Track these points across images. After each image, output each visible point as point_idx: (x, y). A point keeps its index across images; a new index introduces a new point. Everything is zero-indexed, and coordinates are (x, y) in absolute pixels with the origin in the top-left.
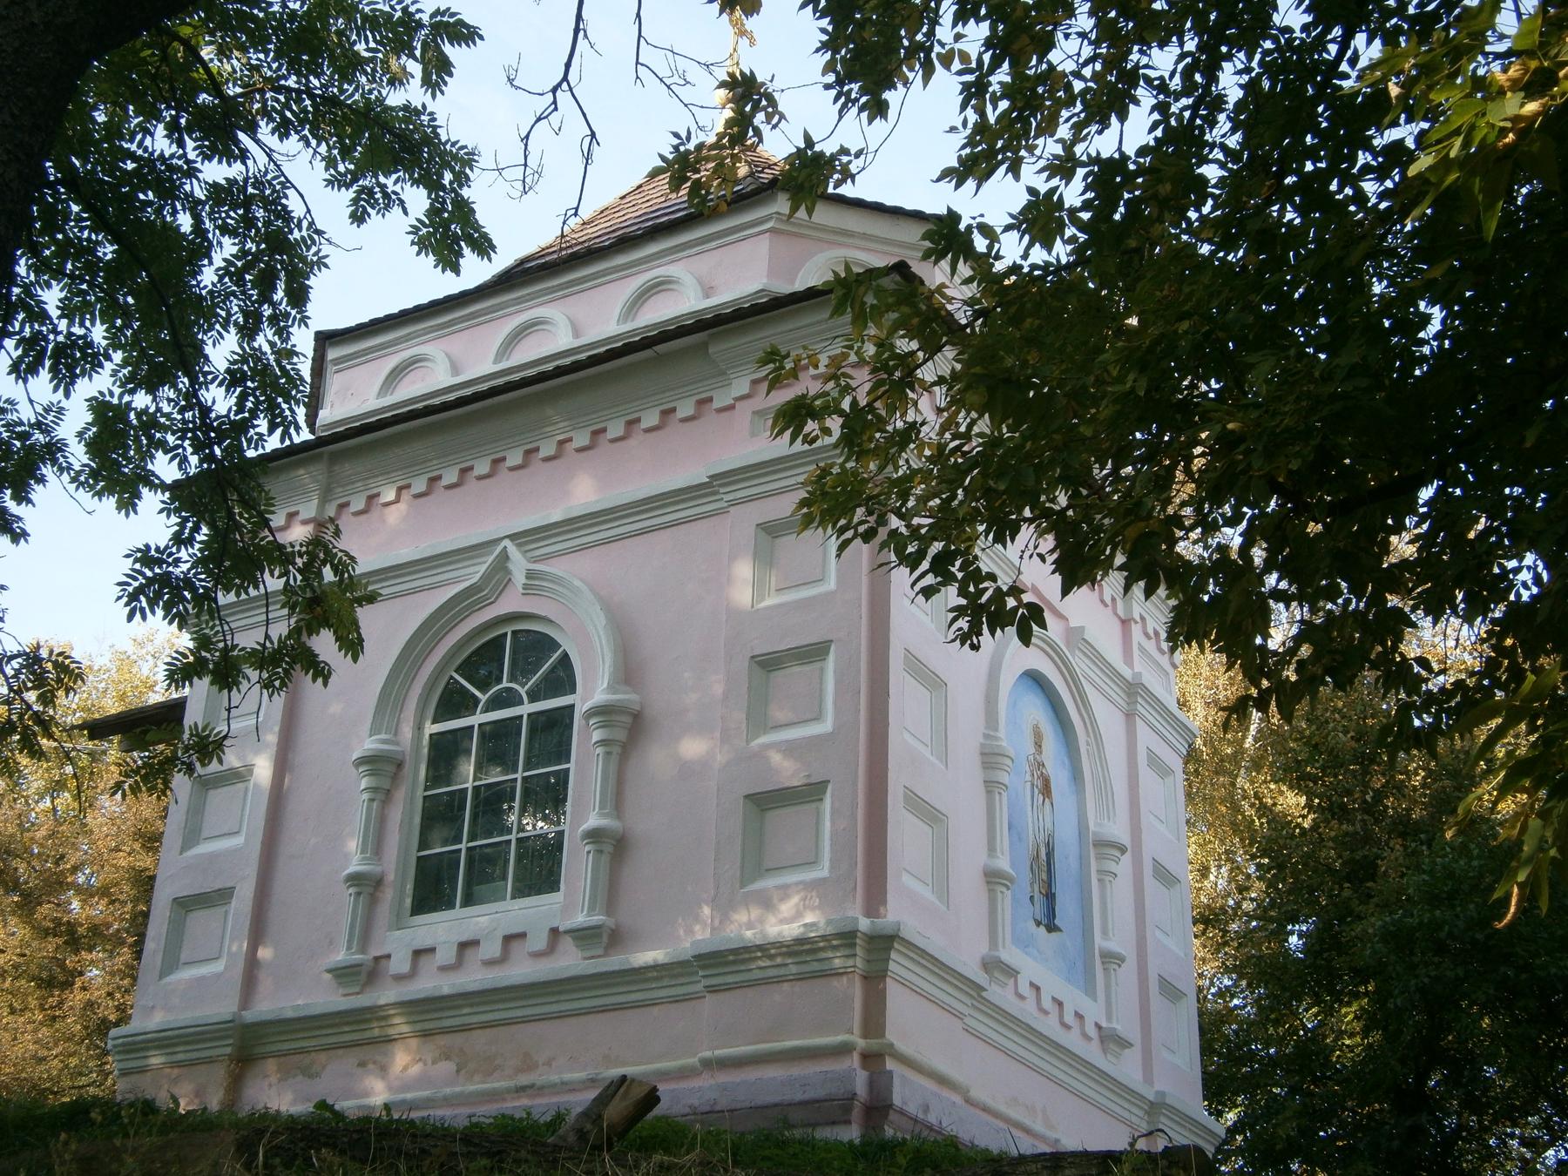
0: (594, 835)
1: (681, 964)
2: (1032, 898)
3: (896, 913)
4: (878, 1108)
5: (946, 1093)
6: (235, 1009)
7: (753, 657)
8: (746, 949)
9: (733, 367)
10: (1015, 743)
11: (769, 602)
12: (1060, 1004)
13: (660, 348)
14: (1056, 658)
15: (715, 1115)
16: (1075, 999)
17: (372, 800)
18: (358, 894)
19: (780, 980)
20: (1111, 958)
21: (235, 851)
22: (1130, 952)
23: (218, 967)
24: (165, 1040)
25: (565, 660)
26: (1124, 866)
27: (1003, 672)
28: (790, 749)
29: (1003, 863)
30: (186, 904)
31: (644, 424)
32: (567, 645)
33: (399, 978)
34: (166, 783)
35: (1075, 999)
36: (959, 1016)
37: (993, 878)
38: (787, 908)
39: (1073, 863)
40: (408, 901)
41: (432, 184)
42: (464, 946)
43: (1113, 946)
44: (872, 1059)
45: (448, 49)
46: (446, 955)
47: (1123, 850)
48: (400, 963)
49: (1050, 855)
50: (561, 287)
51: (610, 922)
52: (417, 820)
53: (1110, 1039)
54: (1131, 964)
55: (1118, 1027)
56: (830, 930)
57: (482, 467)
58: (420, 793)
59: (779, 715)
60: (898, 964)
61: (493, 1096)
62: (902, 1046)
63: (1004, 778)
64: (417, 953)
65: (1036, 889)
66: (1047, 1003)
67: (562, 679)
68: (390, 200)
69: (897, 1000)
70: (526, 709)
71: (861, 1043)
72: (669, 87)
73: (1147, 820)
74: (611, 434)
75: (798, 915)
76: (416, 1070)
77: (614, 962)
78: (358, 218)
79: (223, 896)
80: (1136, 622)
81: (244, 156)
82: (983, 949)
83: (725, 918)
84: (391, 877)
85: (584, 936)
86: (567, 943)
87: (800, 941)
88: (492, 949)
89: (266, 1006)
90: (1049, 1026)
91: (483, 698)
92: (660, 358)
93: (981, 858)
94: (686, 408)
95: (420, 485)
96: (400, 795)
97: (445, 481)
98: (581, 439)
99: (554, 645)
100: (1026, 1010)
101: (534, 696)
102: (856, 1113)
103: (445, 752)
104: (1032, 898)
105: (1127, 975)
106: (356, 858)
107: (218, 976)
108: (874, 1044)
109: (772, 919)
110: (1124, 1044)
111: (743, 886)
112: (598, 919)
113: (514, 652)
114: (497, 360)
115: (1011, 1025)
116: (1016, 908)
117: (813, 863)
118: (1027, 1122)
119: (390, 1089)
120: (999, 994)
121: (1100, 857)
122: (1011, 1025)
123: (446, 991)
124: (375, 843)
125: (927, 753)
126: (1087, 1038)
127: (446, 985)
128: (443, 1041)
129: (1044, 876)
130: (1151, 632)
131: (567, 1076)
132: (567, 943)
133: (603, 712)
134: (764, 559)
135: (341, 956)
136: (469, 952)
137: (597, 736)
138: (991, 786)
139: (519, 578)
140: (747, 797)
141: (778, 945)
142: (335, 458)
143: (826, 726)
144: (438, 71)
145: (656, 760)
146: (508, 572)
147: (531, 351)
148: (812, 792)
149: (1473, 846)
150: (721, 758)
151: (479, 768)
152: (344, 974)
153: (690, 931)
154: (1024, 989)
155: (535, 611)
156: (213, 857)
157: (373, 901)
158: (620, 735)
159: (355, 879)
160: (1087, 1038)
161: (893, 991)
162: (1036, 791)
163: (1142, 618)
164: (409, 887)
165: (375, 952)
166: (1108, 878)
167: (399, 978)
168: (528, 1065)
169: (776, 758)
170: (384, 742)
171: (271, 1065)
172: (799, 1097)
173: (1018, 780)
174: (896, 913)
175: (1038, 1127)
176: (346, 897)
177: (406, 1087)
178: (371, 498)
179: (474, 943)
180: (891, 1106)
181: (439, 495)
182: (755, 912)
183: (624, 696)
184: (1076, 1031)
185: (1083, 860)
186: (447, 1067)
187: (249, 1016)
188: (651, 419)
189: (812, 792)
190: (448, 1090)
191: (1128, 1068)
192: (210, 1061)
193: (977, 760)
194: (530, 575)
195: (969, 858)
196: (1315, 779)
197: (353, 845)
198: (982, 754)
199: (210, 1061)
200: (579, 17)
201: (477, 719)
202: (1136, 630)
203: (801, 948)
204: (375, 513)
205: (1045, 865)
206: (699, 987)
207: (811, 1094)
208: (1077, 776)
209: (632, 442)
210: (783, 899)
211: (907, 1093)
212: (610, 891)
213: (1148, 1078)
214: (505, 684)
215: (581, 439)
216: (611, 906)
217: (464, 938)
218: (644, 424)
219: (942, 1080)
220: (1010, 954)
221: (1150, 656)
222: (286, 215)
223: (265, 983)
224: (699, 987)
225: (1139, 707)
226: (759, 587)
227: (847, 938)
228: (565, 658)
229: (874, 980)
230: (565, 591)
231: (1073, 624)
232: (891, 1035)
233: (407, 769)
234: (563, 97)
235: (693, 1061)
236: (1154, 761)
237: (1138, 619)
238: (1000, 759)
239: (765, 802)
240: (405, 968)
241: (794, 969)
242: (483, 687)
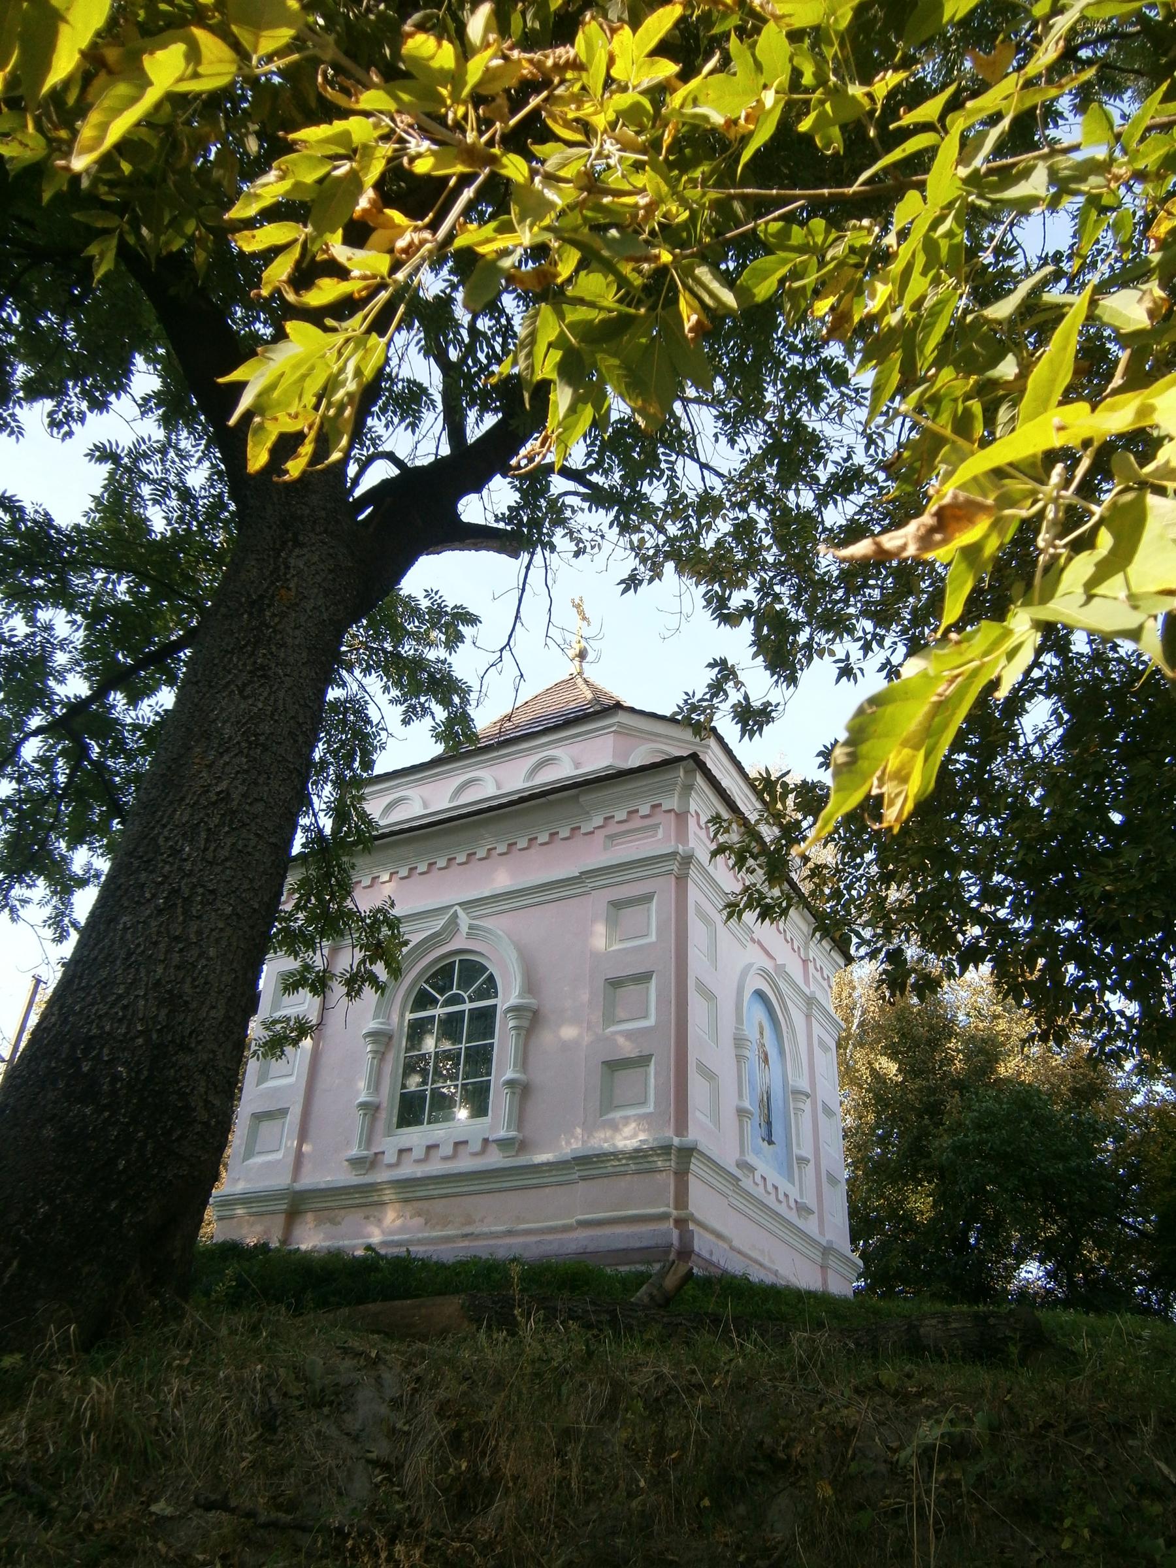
0: (511, 1083)
1: (566, 1162)
3: (694, 1134)
4: (686, 1252)
5: (720, 1243)
6: (288, 1181)
8: (605, 1154)
10: (751, 1033)
11: (615, 947)
12: (776, 1188)
16: (784, 1186)
19: (625, 1174)
20: (802, 1160)
21: (290, 1086)
22: (810, 1156)
23: (278, 1156)
24: (246, 1200)
25: (491, 978)
26: (807, 1106)
28: (629, 1035)
29: (746, 1104)
30: (259, 1118)
31: (540, 841)
32: (492, 969)
33: (390, 1166)
34: (283, 1052)
35: (784, 1186)
36: (725, 1196)
38: (628, 1130)
39: (781, 1104)
40: (395, 1120)
41: (446, 703)
42: (430, 1148)
44: (680, 1223)
45: (461, 627)
46: (418, 1153)
47: (808, 1096)
48: (390, 1157)
49: (768, 1099)
51: (520, 1136)
52: (401, 1071)
53: (803, 1209)
54: (812, 1162)
56: (655, 1144)
57: (442, 863)
58: (402, 1055)
59: (621, 1014)
60: (695, 1165)
61: (447, 1239)
62: (697, 1215)
63: (747, 1053)
64: (401, 1151)
66: (770, 1188)
67: (490, 988)
68: (426, 710)
69: (696, 1188)
70: (467, 1006)
71: (675, 1213)
73: (818, 1078)
74: (519, 846)
75: (635, 1135)
76: (399, 1222)
77: (522, 1160)
78: (406, 722)
79: (283, 1112)
81: (344, 685)
82: (737, 1156)
83: (590, 1135)
84: (385, 1105)
85: (504, 1144)
86: (493, 1148)
87: (637, 1150)
88: (447, 1150)
89: (311, 1179)
90: (771, 1201)
91: (441, 999)
92: (550, 803)
93: (735, 1102)
94: (565, 833)
95: (404, 872)
96: (390, 1056)
97: (419, 870)
98: (502, 848)
99: (485, 969)
100: (759, 1191)
101: (471, 1000)
103: (417, 1030)
105: (810, 1169)
106: (364, 1093)
107: (278, 1161)
108: (682, 1213)
109: (618, 1137)
112: (513, 1134)
113: (460, 971)
114: (451, 800)
116: (753, 1129)
117: (644, 1103)
118: (760, 1258)
119: (383, 1232)
120: (747, 1183)
121: (795, 1100)
123: (419, 1175)
124: (375, 1084)
126: (790, 1208)
127: (419, 1171)
128: (417, 1205)
131: (494, 1229)
132: (493, 1148)
133: (515, 1009)
134: (612, 923)
135: (354, 1152)
136: (433, 1152)
137: (511, 1024)
138: (740, 1058)
139: (464, 929)
141: (622, 1152)
143: (651, 1022)
144: (454, 640)
145: (546, 1038)
146: (457, 925)
147: (471, 796)
148: (642, 1061)
150: (587, 1039)
151: (438, 1040)
152: (357, 1163)
153: (568, 1143)
154: (758, 1179)
155: (735, 986)
157: (374, 1119)
158: (526, 1024)
159: (364, 1106)
160: (790, 1208)
161: (691, 1179)
164: (396, 1111)
167: (390, 1166)
168: (469, 1221)
169: (621, 1040)
171: (310, 1217)
172: (638, 1245)
173: (752, 1054)
174: (694, 1134)
175: (766, 1262)
176: (358, 1116)
177: (392, 1233)
178: (374, 879)
179: (436, 1146)
181: (416, 878)
182: (609, 1133)
184: (784, 1205)
186: (419, 1221)
187: (298, 1186)
188: (544, 837)
189: (642, 1061)
190: (420, 1235)
191: (810, 1226)
192: (273, 1213)
193: (732, 1042)
194: (471, 927)
195: (729, 1102)
197: (362, 1084)
199: (273, 1213)
200: (518, 611)
201: (439, 1011)
202: (811, 965)
203: (637, 1155)
204: (376, 887)
205: (766, 1104)
206: (576, 1176)
207: (644, 1244)
208: (782, 1052)
209: (532, 851)
210: (626, 1125)
211: (702, 1244)
212: (519, 1118)
213: (822, 1233)
215: (502, 848)
216: (519, 1128)
217: (430, 1143)
218: (540, 841)
219: (719, 1236)
220: (751, 1159)
222: (368, 721)
223: (307, 1167)
226: (609, 938)
227: (666, 1149)
228: (491, 977)
229: (682, 1175)
232: (692, 1208)
233: (395, 1040)
234: (506, 653)
235: (573, 1221)
239: (614, 1066)
240: (394, 1160)
241: (633, 1167)
242: (442, 993)
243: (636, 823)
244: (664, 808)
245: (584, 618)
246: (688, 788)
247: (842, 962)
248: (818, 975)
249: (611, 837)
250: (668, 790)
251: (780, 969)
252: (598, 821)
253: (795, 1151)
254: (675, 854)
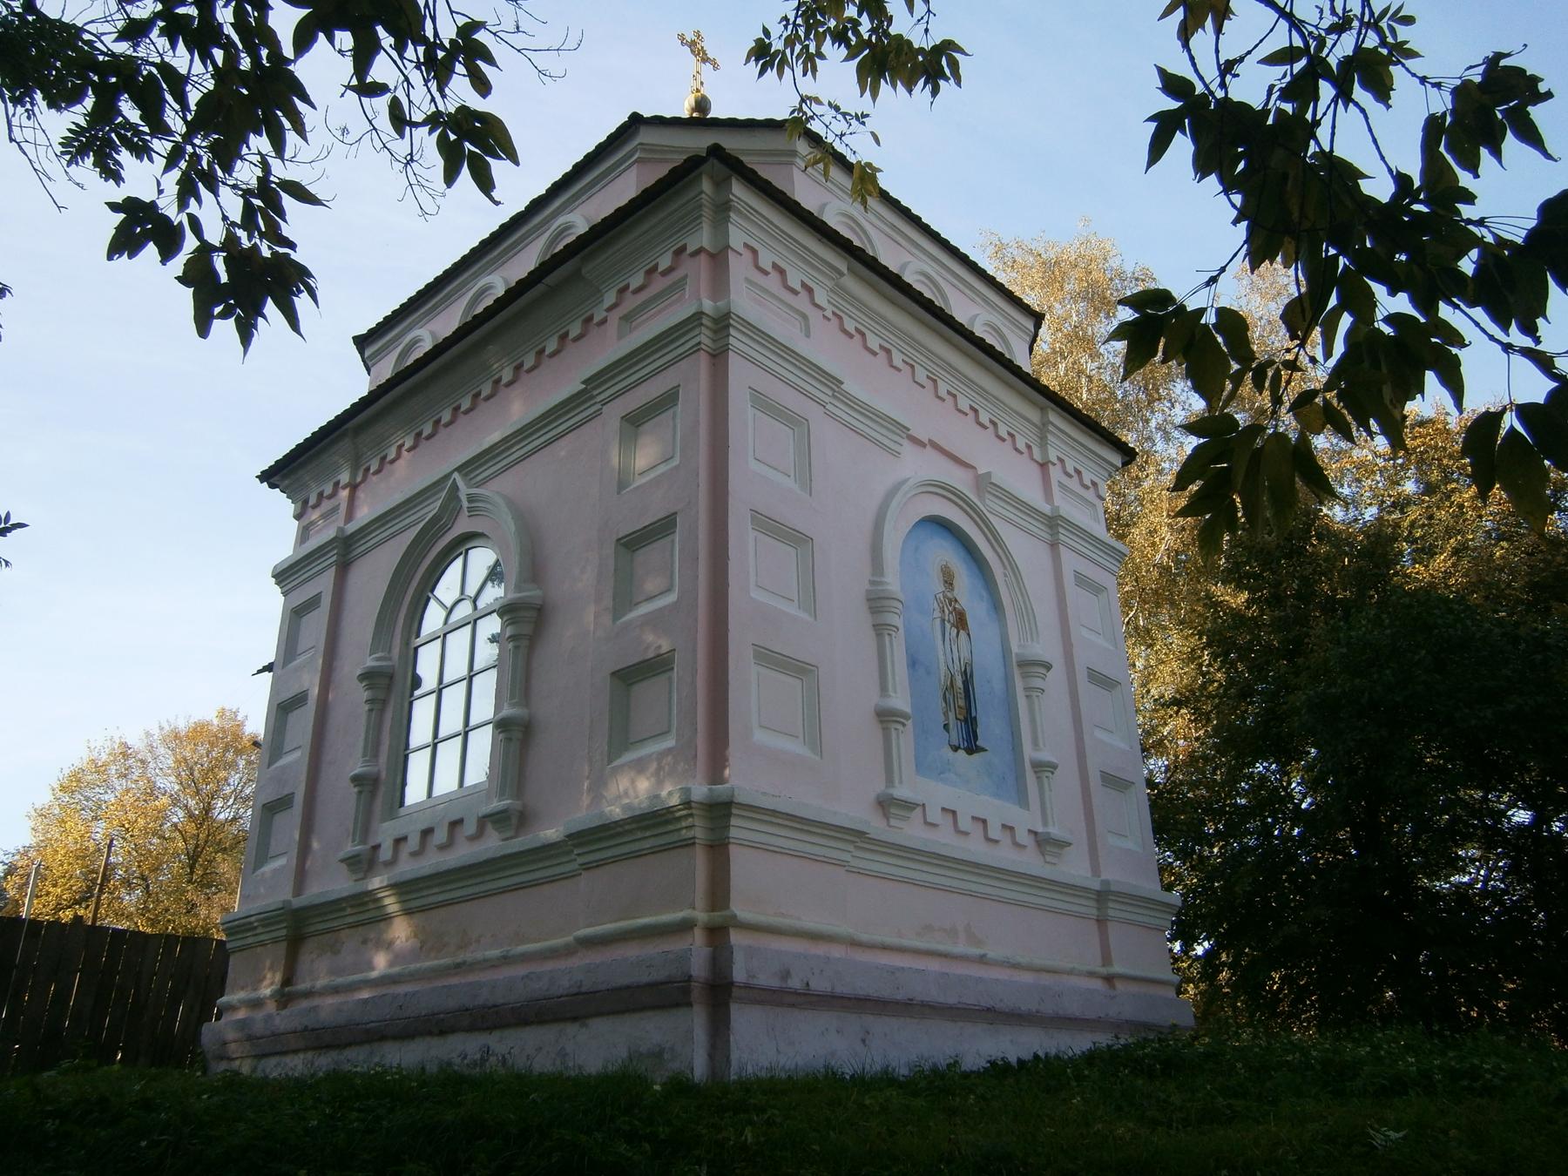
2: (946, 727)
3: (742, 779)
7: (619, 540)
9: (604, 282)
13: (551, 280)
14: (961, 503)
15: (581, 997)
17: (371, 710)
18: (360, 792)
27: (887, 522)
29: (900, 700)
37: (886, 717)
39: (998, 686)
43: (1045, 756)
50: (500, 256)
51: (518, 805)
53: (1045, 843)
55: (1054, 831)
65: (951, 716)
72: (495, 34)
84: (383, 775)
100: (943, 840)
102: (696, 994)
104: (946, 727)
110: (1062, 844)
111: (610, 762)
115: (917, 857)
121: (1025, 676)
122: (917, 857)
125: (792, 610)
129: (962, 703)
130: (1072, 472)
135: (350, 848)
138: (880, 629)
140: (614, 674)
142: (358, 430)
149: (1384, 616)
156: (283, 768)
157: (373, 794)
159: (357, 780)
162: (948, 626)
163: (1029, 447)
165: (372, 843)
166: (1034, 694)
170: (378, 659)
172: (645, 979)
180: (732, 984)
183: (532, 593)
185: (1008, 680)
190: (413, 967)
196: (1256, 577)
198: (868, 600)
202: (1055, 473)
203: (654, 820)
213: (1096, 871)
221: (1072, 492)
224: (575, 866)
225: (1062, 537)
229: (718, 849)
230: (488, 506)
231: (981, 471)
236: (1081, 580)
237: (1056, 461)
238: (886, 603)
243: (659, 284)
244: (690, 249)
245: (705, 60)
246: (723, 209)
247: (1117, 460)
248: (1073, 484)
249: (627, 318)
250: (691, 221)
251: (984, 483)
252: (610, 298)
253: (1028, 752)
254: (699, 315)
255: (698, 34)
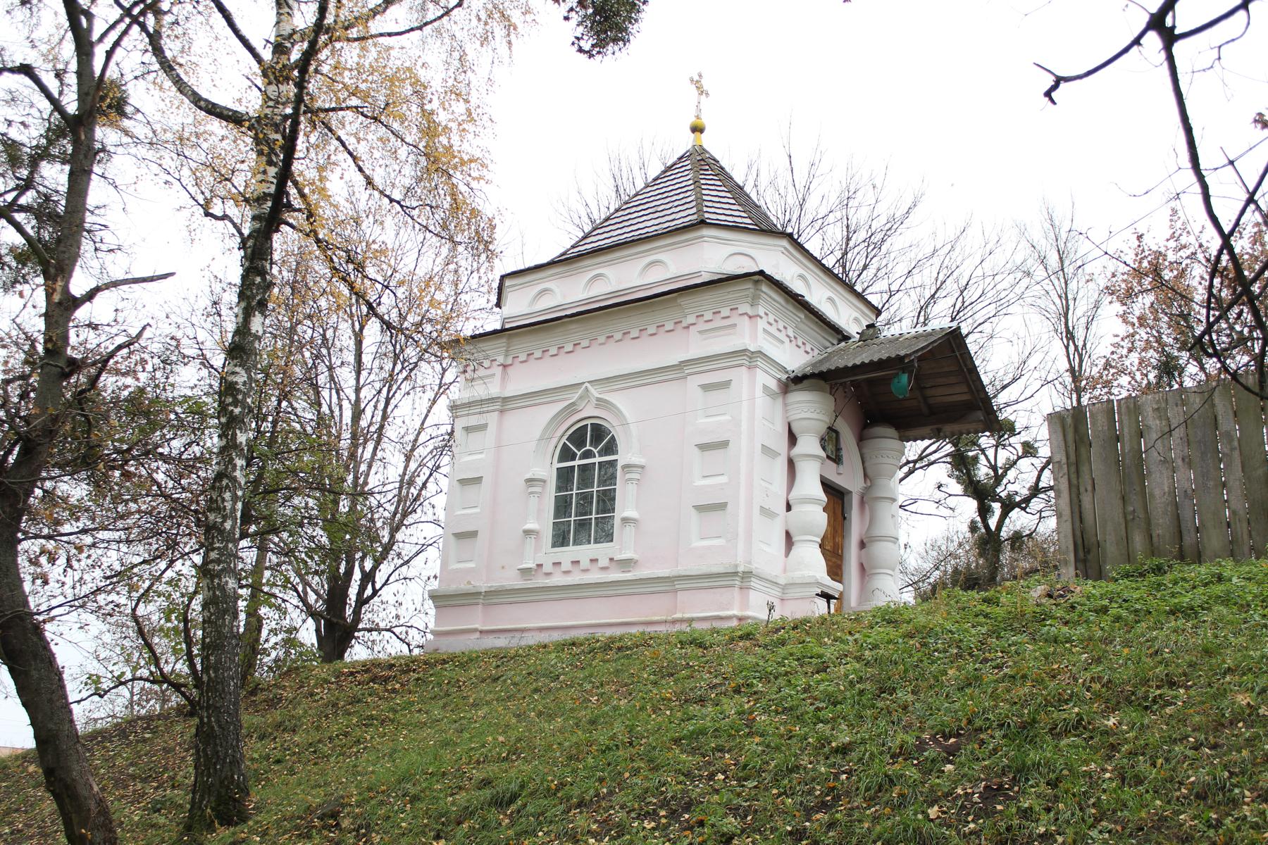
70: (597, 460)
80: (761, 317)
214: (588, 447)
255: (700, 76)
